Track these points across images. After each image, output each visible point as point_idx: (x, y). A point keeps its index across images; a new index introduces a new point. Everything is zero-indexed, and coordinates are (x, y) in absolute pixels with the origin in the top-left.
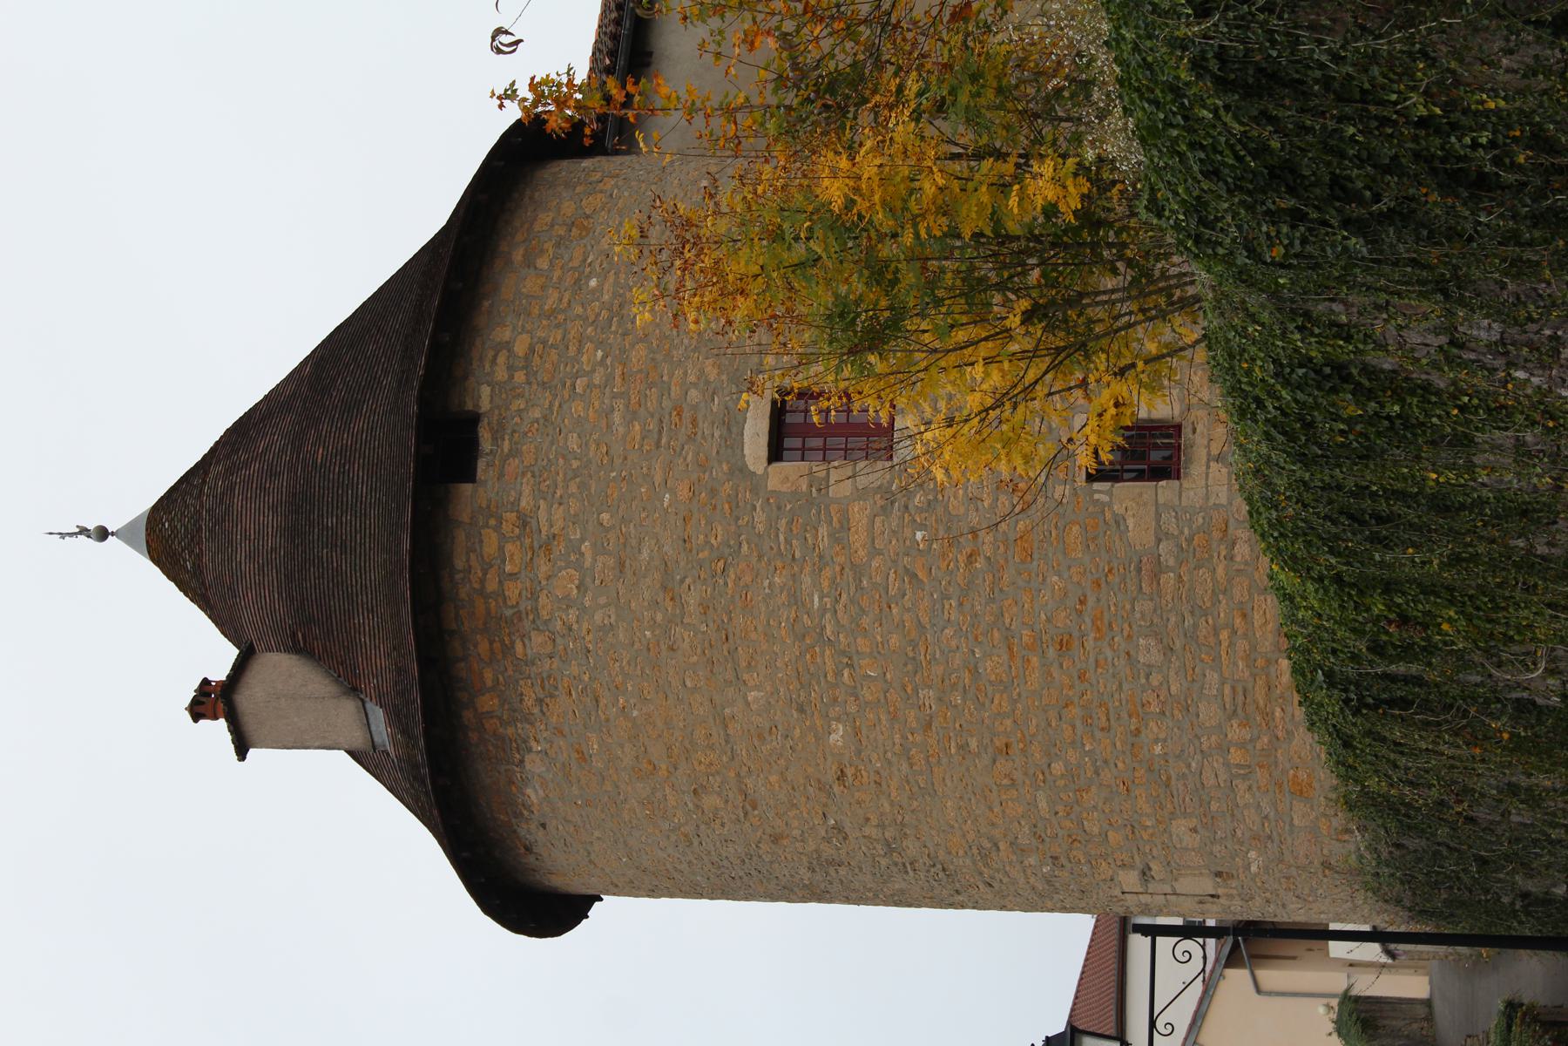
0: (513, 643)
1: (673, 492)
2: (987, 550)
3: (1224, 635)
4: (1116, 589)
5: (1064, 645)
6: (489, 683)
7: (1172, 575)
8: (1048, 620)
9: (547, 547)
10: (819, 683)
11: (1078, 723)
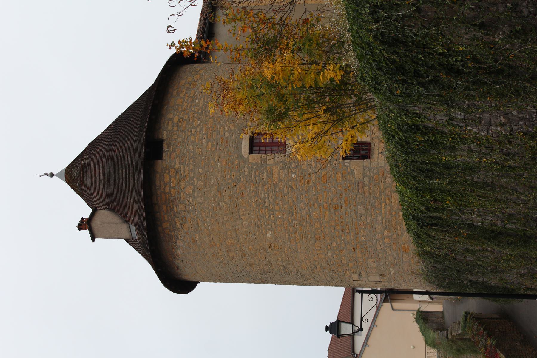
0: (173, 207)
1: (221, 163)
2: (313, 180)
3: (383, 205)
4: (351, 191)
5: (336, 208)
6: (166, 219)
7: (368, 187)
8: (331, 201)
9: (183, 179)
10: (264, 219)
11: (340, 231)
